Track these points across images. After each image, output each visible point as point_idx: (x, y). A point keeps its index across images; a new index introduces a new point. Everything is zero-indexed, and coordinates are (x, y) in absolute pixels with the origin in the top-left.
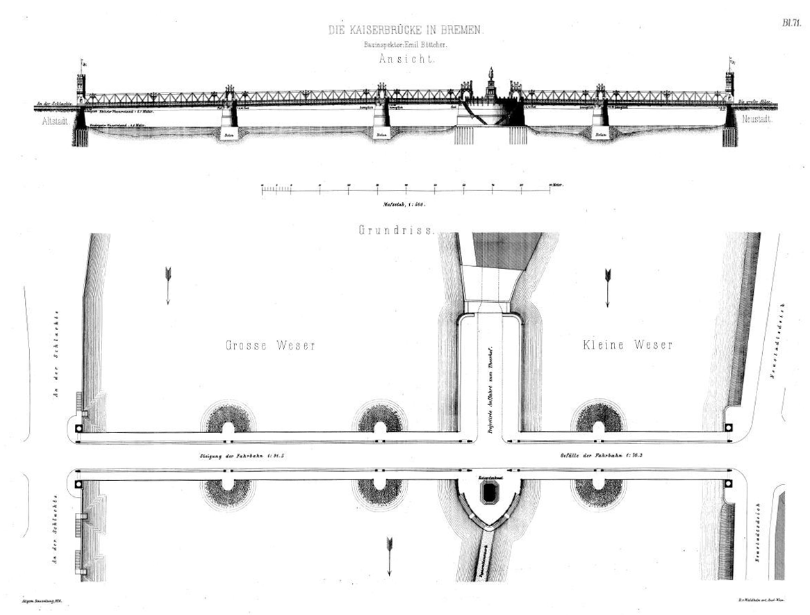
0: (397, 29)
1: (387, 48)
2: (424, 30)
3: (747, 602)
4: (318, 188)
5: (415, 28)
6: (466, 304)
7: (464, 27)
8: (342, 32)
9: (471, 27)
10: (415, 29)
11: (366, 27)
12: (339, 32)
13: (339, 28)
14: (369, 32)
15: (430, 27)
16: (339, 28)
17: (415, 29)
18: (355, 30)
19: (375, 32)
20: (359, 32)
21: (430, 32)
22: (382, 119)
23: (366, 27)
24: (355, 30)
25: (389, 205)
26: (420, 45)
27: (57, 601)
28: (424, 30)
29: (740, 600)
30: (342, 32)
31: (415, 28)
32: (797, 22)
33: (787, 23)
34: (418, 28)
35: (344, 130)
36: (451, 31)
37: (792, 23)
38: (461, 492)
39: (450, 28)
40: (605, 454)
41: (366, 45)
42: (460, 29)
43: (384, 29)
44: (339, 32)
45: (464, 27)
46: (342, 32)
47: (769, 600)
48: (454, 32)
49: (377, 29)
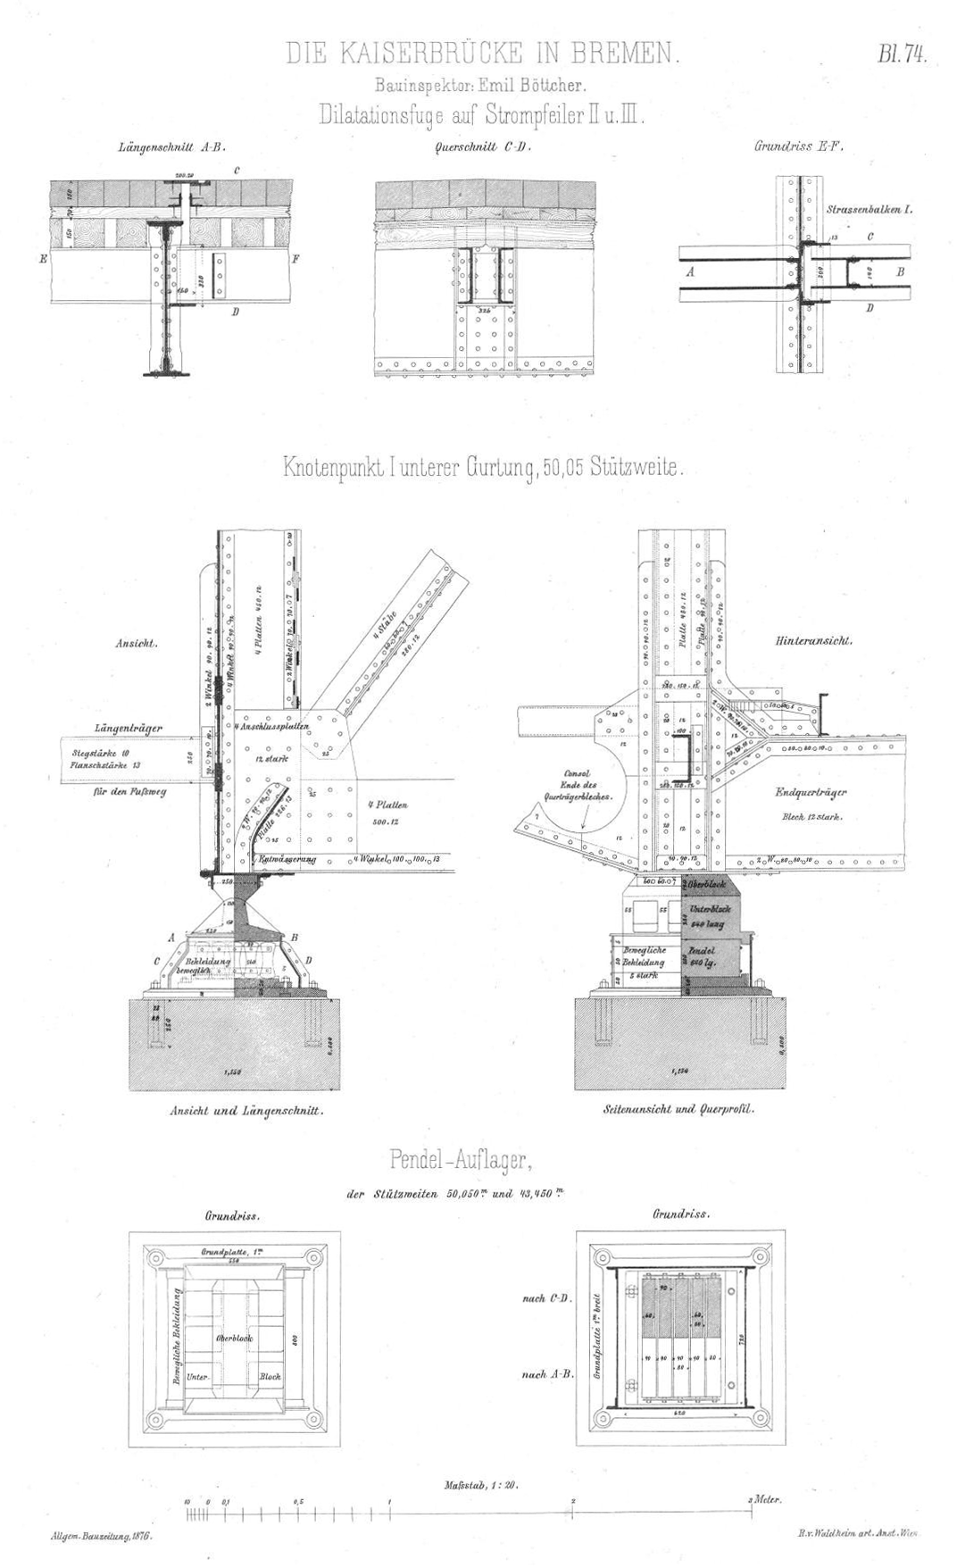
0: (460, 52)
1: (433, 92)
2: (530, 53)
3: (820, 1539)
5: (507, 46)
7: (630, 47)
10: (506, 50)
11: (380, 46)
12: (312, 58)
13: (312, 46)
14: (389, 58)
15: (544, 47)
16: (312, 46)
18: (355, 51)
19: (405, 59)
21: (544, 59)
22: (695, 760)
23: (380, 46)
24: (355, 51)
25: (455, 1487)
26: (517, 86)
27: (136, 1536)
28: (530, 53)
29: (802, 1533)
30: (320, 58)
32: (916, 51)
33: (888, 54)
34: (320, 46)
36: (421, 56)
37: (902, 53)
38: (174, 178)
42: (619, 52)
43: (428, 51)
44: (312, 58)
45: (630, 47)
46: (321, 59)
47: (882, 1533)
48: (605, 58)
49: (411, 52)
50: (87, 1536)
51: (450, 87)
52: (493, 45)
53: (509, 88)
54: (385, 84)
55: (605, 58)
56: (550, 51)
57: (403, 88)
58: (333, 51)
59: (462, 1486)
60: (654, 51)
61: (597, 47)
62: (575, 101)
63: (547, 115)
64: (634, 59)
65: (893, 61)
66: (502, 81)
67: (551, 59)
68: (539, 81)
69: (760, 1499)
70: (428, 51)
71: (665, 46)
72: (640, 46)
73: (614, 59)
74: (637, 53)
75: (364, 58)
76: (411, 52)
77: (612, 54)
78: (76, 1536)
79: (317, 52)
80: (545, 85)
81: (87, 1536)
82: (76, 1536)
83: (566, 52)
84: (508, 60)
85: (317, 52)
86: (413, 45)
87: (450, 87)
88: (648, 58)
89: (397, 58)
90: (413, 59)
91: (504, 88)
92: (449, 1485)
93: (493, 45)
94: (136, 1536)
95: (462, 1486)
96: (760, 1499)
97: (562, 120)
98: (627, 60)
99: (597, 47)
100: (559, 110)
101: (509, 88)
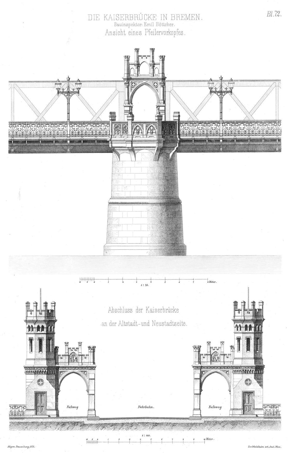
4: (193, 441)
6: (194, 416)
7: (188, 16)
8: (98, 19)
9: (122, 16)
10: (152, 17)
13: (95, 16)
15: (163, 16)
17: (152, 17)
18: (108, 17)
20: (110, 19)
24: (108, 17)
27: (31, 447)
31: (152, 16)
33: (270, 14)
34: (98, 16)
35: (104, 419)
36: (178, 18)
37: (274, 14)
39: (136, 16)
40: (144, 406)
41: (175, 310)
42: (184, 17)
43: (129, 17)
44: (191, 19)
45: (188, 16)
48: (181, 19)
50: (17, 447)
51: (136, 25)
52: (148, 15)
53: (153, 25)
54: (117, 24)
55: (181, 19)
56: (165, 17)
57: (122, 25)
58: (102, 17)
59: (214, 407)
60: (195, 17)
61: (178, 16)
62: (172, 29)
63: (178, 32)
64: (189, 19)
65: (190, 20)
66: (151, 23)
67: (165, 19)
68: (161, 23)
69: (207, 439)
70: (129, 17)
71: (198, 15)
72: (191, 15)
73: (122, 19)
74: (189, 17)
75: (110, 19)
76: (124, 17)
77: (122, 18)
78: (14, 447)
79: (96, 17)
80: (163, 24)
81: (17, 447)
82: (14, 447)
83: (169, 17)
84: (152, 19)
85: (96, 17)
86: (125, 15)
87: (136, 25)
88: (183, 19)
89: (120, 19)
90: (125, 19)
91: (151, 25)
92: (210, 407)
93: (148, 15)
94: (31, 447)
95: (214, 407)
96: (207, 439)
97: (155, 34)
98: (187, 19)
99: (131, 16)
100: (153, 31)
101: (153, 25)
